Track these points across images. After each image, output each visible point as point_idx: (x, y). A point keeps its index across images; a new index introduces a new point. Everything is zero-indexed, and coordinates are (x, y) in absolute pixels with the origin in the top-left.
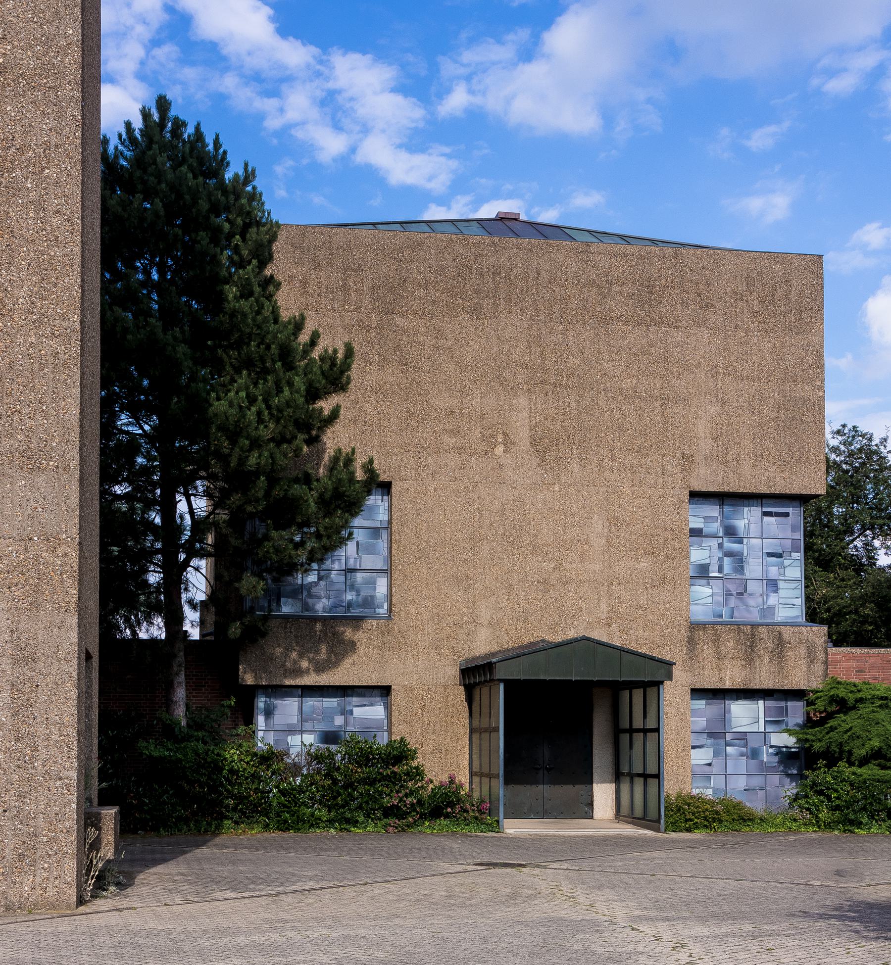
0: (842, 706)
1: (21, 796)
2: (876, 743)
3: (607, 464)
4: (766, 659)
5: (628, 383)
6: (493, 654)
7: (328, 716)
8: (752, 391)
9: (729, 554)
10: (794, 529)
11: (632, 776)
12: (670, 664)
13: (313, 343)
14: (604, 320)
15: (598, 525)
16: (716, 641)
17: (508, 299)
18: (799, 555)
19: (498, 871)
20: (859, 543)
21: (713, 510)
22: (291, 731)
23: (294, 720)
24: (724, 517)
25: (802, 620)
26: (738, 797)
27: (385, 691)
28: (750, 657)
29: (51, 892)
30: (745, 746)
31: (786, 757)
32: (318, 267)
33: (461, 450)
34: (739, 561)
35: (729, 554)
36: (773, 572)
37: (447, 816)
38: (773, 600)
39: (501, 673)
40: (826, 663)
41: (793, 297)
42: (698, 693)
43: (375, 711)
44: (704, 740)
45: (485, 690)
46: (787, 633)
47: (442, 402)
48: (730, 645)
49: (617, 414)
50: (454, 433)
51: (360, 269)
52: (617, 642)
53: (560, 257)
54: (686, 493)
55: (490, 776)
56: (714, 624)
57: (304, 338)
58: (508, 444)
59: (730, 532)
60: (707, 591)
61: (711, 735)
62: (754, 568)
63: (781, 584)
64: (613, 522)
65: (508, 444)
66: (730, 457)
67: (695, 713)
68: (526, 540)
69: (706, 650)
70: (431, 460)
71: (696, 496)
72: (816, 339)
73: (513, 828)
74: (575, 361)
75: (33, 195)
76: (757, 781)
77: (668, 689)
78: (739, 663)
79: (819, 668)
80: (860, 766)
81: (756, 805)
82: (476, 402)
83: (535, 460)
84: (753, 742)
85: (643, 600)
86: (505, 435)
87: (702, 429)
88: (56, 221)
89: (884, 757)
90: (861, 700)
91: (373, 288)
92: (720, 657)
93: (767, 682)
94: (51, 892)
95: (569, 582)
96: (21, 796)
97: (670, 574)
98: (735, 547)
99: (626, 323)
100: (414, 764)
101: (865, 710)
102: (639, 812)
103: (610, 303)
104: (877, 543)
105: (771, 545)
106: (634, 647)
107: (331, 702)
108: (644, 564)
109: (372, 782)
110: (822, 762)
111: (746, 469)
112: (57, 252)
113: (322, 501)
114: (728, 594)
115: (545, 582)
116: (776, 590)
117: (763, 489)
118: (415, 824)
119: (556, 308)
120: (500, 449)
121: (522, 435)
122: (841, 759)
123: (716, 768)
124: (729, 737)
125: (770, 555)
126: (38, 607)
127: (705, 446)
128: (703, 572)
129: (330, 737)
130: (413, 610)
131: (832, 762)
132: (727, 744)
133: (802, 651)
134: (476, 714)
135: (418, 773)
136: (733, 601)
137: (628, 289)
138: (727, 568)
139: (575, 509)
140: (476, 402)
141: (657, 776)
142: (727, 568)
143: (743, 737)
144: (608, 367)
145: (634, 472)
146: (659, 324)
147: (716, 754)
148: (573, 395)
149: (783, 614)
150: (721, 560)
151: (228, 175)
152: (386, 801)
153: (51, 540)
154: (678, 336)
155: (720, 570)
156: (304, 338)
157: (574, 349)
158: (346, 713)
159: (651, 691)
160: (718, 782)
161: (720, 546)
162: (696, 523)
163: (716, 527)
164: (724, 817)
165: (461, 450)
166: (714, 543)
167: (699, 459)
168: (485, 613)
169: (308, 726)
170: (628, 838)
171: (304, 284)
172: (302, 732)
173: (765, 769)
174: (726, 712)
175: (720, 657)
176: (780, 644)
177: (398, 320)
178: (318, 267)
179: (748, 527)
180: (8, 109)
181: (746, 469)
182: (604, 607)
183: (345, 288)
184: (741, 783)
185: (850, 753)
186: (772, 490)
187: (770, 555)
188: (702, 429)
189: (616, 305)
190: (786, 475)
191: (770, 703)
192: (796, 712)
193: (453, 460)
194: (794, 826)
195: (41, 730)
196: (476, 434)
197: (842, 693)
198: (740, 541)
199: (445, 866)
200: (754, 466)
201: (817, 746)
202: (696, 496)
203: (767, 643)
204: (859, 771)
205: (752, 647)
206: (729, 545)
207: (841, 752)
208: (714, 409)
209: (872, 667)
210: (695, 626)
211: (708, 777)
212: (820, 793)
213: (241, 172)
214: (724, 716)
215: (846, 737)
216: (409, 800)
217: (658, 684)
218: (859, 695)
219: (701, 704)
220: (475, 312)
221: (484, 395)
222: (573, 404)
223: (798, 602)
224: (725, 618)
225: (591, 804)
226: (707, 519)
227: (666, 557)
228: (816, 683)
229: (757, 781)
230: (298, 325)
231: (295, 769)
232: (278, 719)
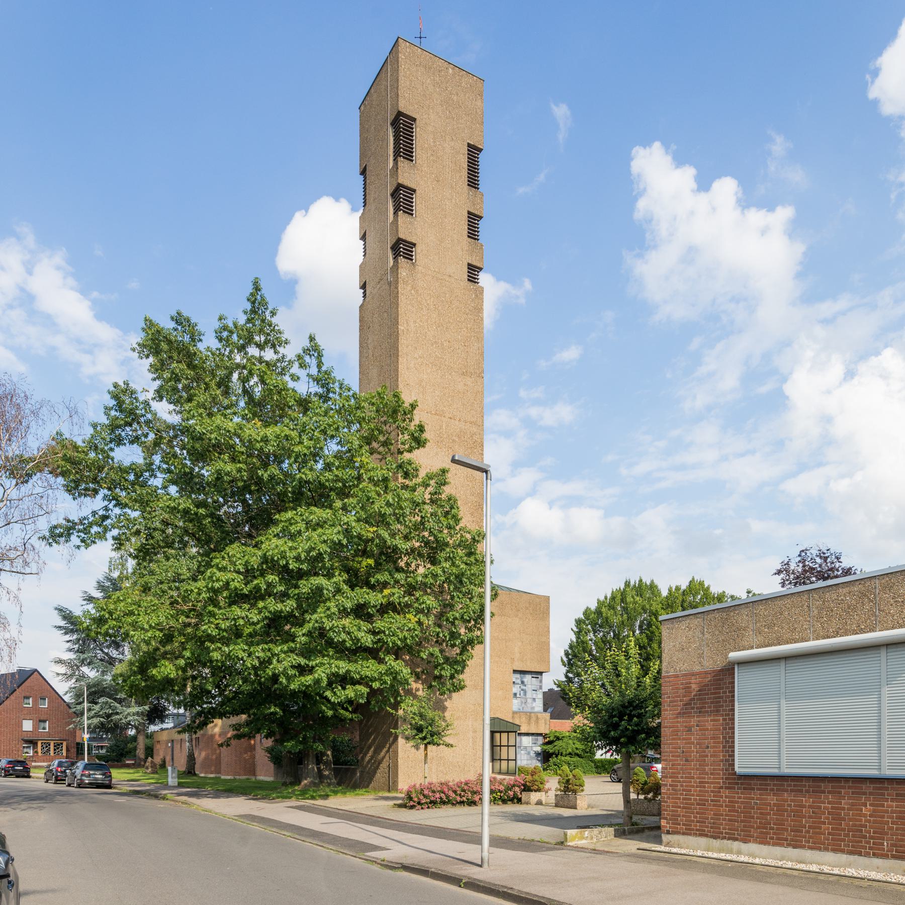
0: (558, 739)
2: (570, 750)
12: (520, 726)
16: (520, 717)
21: (518, 676)
24: (522, 678)
31: (537, 754)
34: (525, 692)
38: (534, 705)
46: (539, 715)
59: (523, 682)
62: (530, 694)
71: (515, 671)
84: (529, 749)
90: (563, 737)
98: (524, 687)
108: (500, 693)
114: (522, 702)
117: (533, 670)
133: (543, 721)
136: (523, 705)
138: (522, 694)
142: (522, 694)
149: (536, 709)
154: (510, 620)
163: (519, 681)
166: (518, 686)
167: (516, 659)
173: (531, 758)
176: (537, 718)
180: (371, 562)
188: (516, 650)
191: (534, 737)
192: (541, 740)
202: (515, 671)
203: (534, 719)
205: (530, 719)
206: (523, 687)
208: (520, 644)
210: (514, 713)
212: (556, 765)
226: (516, 678)
228: (547, 732)
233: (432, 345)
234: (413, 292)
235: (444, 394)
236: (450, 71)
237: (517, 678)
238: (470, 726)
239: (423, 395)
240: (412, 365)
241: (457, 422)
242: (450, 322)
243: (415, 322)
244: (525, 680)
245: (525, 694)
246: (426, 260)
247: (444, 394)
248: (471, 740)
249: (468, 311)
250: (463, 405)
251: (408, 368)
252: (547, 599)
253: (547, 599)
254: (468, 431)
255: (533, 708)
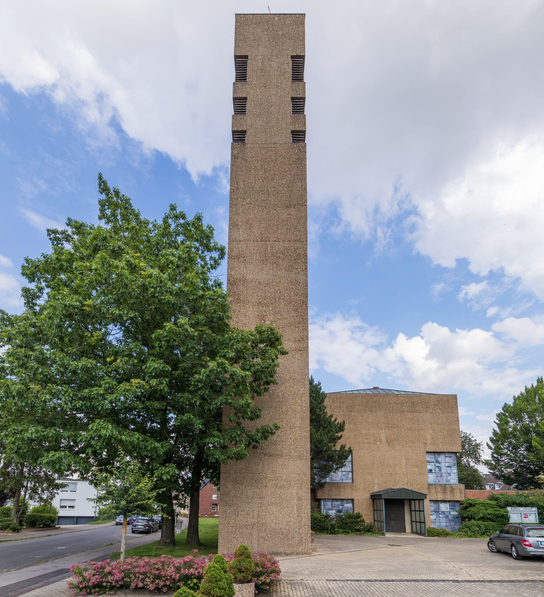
0: (471, 505)
1: (299, 529)
2: (481, 515)
3: (405, 445)
4: (449, 493)
5: (409, 426)
6: (382, 491)
7: (338, 505)
8: (441, 427)
9: (437, 467)
10: (454, 460)
11: (377, 510)
13: (335, 420)
14: (403, 412)
15: (403, 461)
16: (435, 488)
17: (379, 408)
18: (456, 467)
19: (394, 547)
20: (465, 460)
22: (330, 510)
23: (330, 507)
25: (457, 483)
26: (445, 528)
27: (353, 500)
28: (444, 492)
29: (306, 550)
30: (445, 515)
32: (334, 402)
33: (369, 443)
35: (437, 467)
36: (449, 471)
37: (371, 532)
38: (449, 478)
39: (383, 497)
40: (465, 494)
41: (450, 405)
42: (431, 501)
43: (350, 505)
44: (433, 513)
45: (378, 501)
46: (454, 486)
47: (364, 432)
48: (439, 489)
49: (407, 434)
50: (367, 439)
51: (343, 402)
52: (410, 489)
53: (391, 398)
54: (425, 452)
55: (381, 522)
56: (435, 484)
57: (333, 420)
58: (380, 441)
60: (432, 476)
61: (435, 512)
62: (443, 470)
63: (451, 474)
64: (407, 459)
65: (380, 441)
66: (436, 443)
67: (431, 506)
68: (386, 464)
69: (433, 491)
70: (362, 446)
72: (456, 415)
73: (388, 535)
74: (395, 421)
75: (300, 404)
76: (448, 524)
77: (425, 500)
78: (442, 494)
79: (463, 495)
80: (478, 521)
81: (449, 530)
82: (372, 432)
83: (387, 445)
84: (447, 514)
85: (416, 478)
86: (379, 439)
87: (429, 436)
88: (304, 408)
89: (484, 519)
90: (476, 504)
91: (347, 407)
92: (437, 492)
93: (450, 499)
94: (306, 550)
95: (397, 474)
96: (299, 529)
97: (422, 472)
99: (408, 412)
100: (362, 519)
101: (477, 506)
102: (419, 531)
103: (404, 408)
104: (470, 460)
105: (447, 464)
106: (414, 490)
107: (339, 503)
108: (416, 469)
109: (352, 523)
110: (467, 520)
111: (440, 446)
112: (304, 414)
113: (339, 457)
115: (391, 474)
116: (450, 475)
117: (445, 451)
118: (363, 533)
119: (391, 409)
120: (378, 443)
121: (384, 439)
122: (472, 519)
123: (437, 520)
124: (440, 512)
125: (448, 467)
126: (302, 488)
127: (430, 441)
128: (431, 471)
129: (339, 511)
130: (358, 481)
131: (470, 520)
132: (440, 514)
133: (458, 491)
134: (375, 505)
135: (363, 521)
137: (408, 405)
139: (397, 456)
140: (372, 432)
141: (424, 523)
143: (444, 512)
144: (404, 423)
145: (412, 447)
146: (416, 412)
147: (437, 517)
148: (396, 429)
150: (435, 468)
151: (315, 383)
152: (356, 528)
153: (305, 474)
154: (421, 415)
155: (435, 471)
156: (333, 420)
157: (395, 419)
158: (342, 505)
159: (421, 502)
160: (438, 524)
161: (435, 465)
162: (428, 459)
164: (442, 533)
165: (369, 443)
166: (433, 464)
167: (428, 444)
168: (376, 481)
169: (333, 508)
170: (417, 538)
171: (331, 406)
172: (332, 510)
174: (439, 506)
175: (437, 492)
177: (353, 414)
178: (334, 402)
179: (441, 460)
181: (440, 446)
182: (406, 480)
183: (340, 407)
184: (444, 524)
185: (474, 517)
186: (448, 451)
187: (448, 467)
188: (429, 436)
189: (405, 408)
190: (451, 447)
193: (367, 445)
194: (461, 536)
195: (303, 515)
196: (372, 439)
197: (470, 502)
198: (440, 463)
199: (380, 545)
200: (443, 445)
201: (465, 515)
203: (449, 489)
204: (477, 522)
206: (437, 464)
207: (472, 517)
208: (431, 432)
209: (477, 495)
210: (429, 485)
211: (435, 522)
212: (468, 528)
213: (318, 383)
214: (439, 507)
215: (473, 513)
216: (362, 527)
217: (423, 500)
218: (475, 502)
219: (432, 504)
220: (371, 411)
221: (374, 430)
222: (396, 432)
223: (456, 478)
224: (437, 483)
225: (405, 529)
227: (421, 467)
229: (448, 524)
230: (331, 416)
231: (333, 519)
232: (327, 507)
233: (259, 193)
234: (243, 162)
235: (270, 225)
236: (277, 18)
237: (429, 458)
238: (295, 495)
239: (250, 229)
240: (240, 211)
241: (281, 243)
242: (274, 174)
243: (244, 181)
244: (440, 459)
245: (440, 470)
246: (254, 139)
247: (270, 225)
248: (295, 507)
249: (291, 162)
250: (287, 229)
251: (237, 214)
252: (455, 397)
253: (455, 397)
254: (292, 248)
255: (449, 481)
